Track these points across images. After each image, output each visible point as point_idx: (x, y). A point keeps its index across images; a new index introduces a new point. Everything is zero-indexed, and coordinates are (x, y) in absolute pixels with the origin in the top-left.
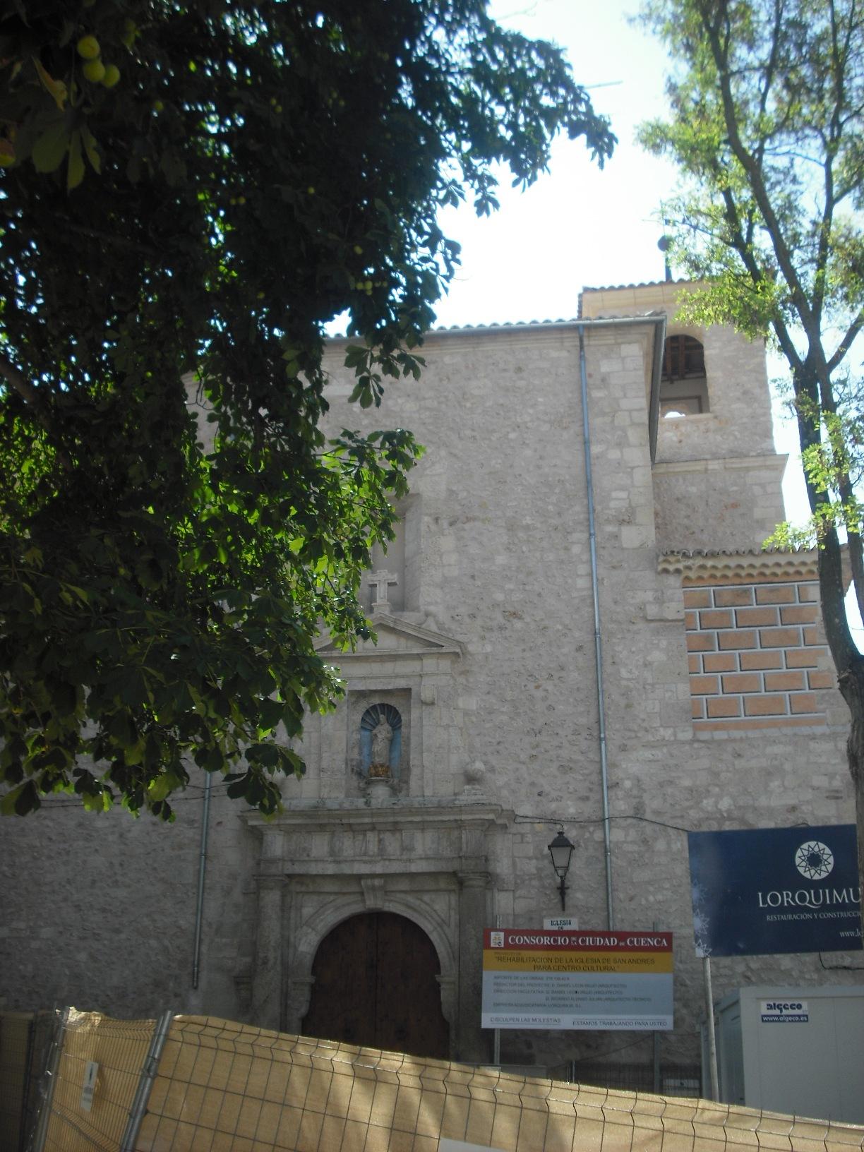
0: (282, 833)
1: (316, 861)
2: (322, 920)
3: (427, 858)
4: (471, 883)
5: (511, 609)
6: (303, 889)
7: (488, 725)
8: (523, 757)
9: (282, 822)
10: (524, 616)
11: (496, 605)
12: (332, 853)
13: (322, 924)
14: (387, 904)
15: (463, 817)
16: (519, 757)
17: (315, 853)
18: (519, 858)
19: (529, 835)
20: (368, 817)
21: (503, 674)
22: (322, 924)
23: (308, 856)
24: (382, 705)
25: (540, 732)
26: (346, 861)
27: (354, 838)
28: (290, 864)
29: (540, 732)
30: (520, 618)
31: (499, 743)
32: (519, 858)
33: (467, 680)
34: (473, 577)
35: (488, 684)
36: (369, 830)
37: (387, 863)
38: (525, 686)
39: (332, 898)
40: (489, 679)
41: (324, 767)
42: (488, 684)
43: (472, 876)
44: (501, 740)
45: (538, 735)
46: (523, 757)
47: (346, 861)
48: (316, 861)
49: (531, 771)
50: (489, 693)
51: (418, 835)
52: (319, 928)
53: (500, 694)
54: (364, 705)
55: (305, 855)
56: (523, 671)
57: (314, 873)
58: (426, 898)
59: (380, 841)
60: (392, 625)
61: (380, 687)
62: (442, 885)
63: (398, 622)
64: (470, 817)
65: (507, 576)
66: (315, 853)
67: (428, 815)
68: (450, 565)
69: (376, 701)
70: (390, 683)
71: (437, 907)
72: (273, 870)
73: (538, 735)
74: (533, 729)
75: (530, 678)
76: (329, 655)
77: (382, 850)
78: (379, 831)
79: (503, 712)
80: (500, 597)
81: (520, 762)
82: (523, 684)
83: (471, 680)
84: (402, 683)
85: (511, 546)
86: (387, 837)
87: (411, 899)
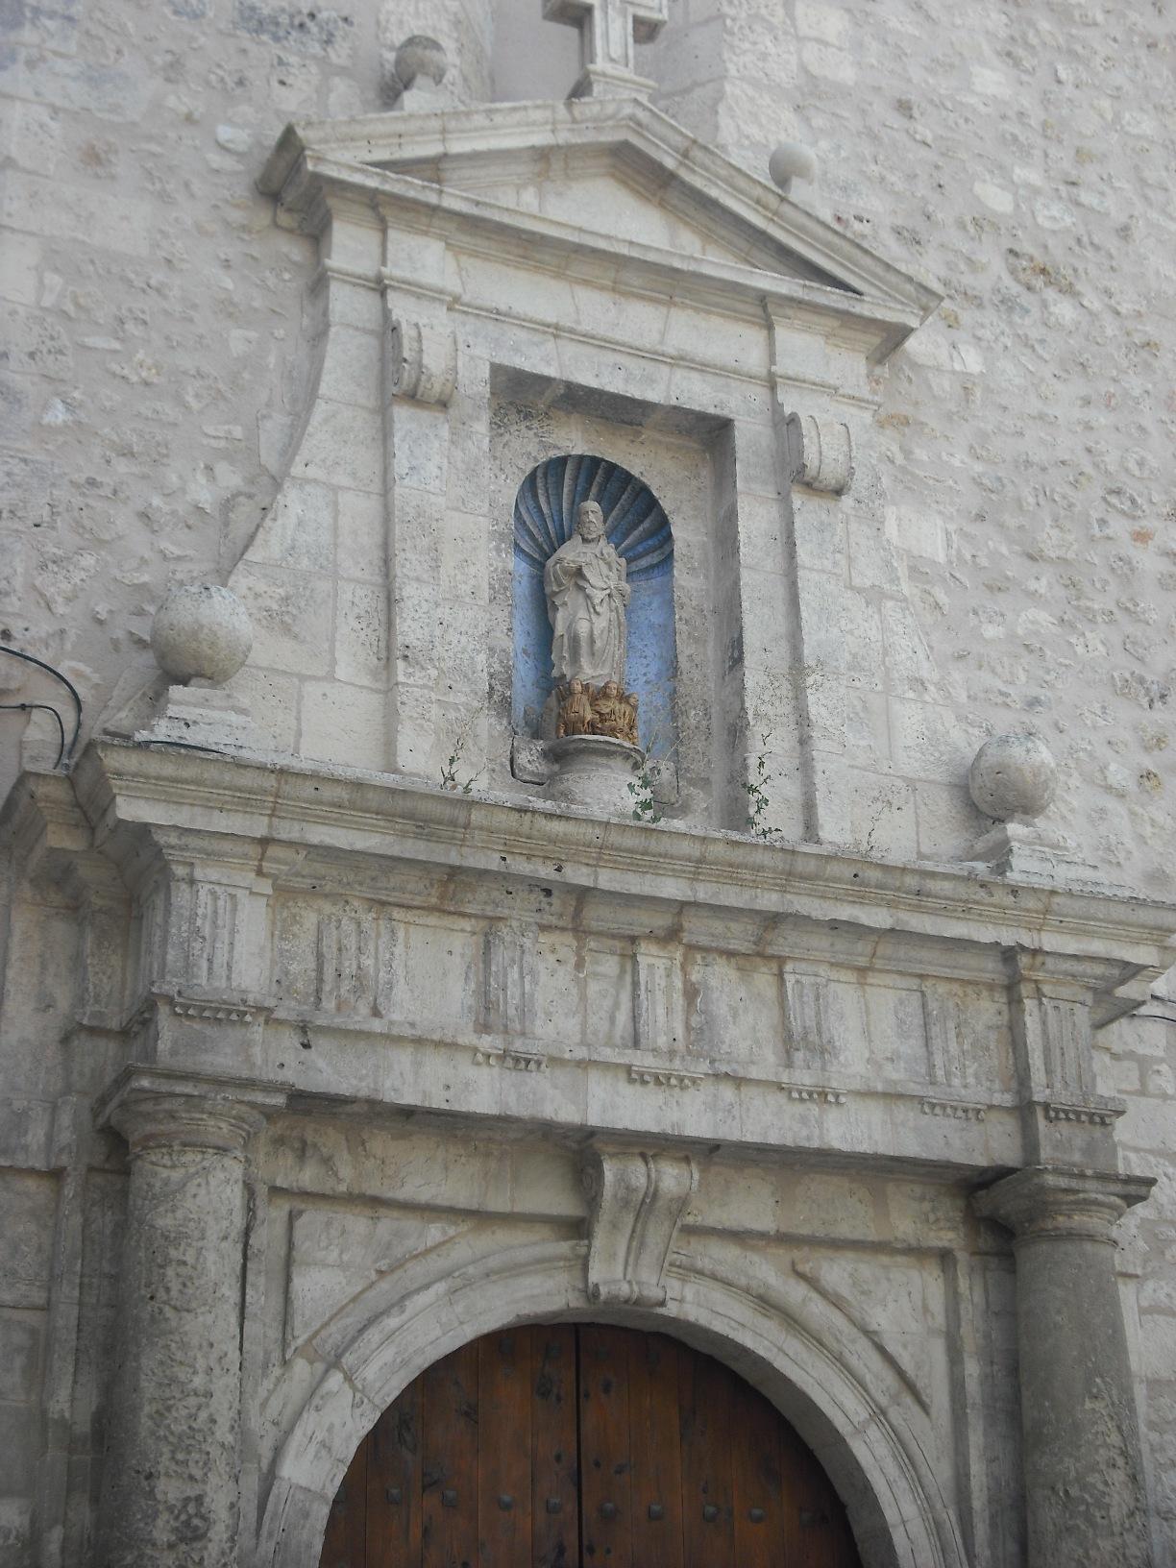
0: (265, 887)
1: (419, 1042)
2: (389, 1337)
3: (892, 1096)
4: (1079, 1220)
5: (1040, 259)
6: (308, 1176)
7: (991, 631)
8: (1119, 774)
9: (288, 830)
10: (1079, 287)
11: (982, 223)
12: (487, 1014)
13: (388, 1354)
14: (674, 1287)
15: (1050, 941)
16: (1103, 769)
17: (405, 1008)
18: (1136, 1150)
19: (1164, 1068)
20: (676, 874)
21: (1028, 463)
22: (388, 1354)
23: (376, 1013)
24: (591, 466)
25: (1163, 696)
26: (556, 1061)
27: (579, 965)
28: (291, 1039)
29: (1163, 696)
30: (1069, 291)
31: (1033, 703)
32: (1136, 1150)
33: (907, 453)
34: (904, 107)
35: (977, 482)
36: (651, 936)
37: (727, 1093)
38: (1102, 522)
39: (435, 1232)
40: (978, 468)
41: (411, 640)
42: (977, 482)
43: (1093, 1190)
44: (1035, 691)
45: (1158, 704)
46: (1119, 774)
47: (556, 1061)
48: (419, 1042)
49: (1148, 830)
50: (981, 517)
51: (844, 994)
52: (370, 1373)
53: (1021, 528)
54: (529, 448)
55: (364, 1009)
56: (1089, 470)
57: (409, 1098)
58: (836, 1272)
59: (691, 993)
60: (670, 163)
61: (614, 384)
62: (904, 1225)
63: (697, 154)
64: (1071, 946)
65: (1015, 138)
66: (405, 1008)
67: (918, 909)
68: (823, 43)
69: (574, 440)
70: (651, 381)
71: (880, 1319)
72: (222, 1057)
73: (1158, 704)
74: (1141, 681)
75: (1113, 499)
76: (432, 199)
77: (701, 1034)
78: (691, 948)
79: (1032, 595)
80: (998, 200)
81: (1109, 788)
82: (1095, 515)
83: (921, 454)
84: (699, 394)
85: (1020, 52)
86: (720, 979)
87: (766, 1271)
